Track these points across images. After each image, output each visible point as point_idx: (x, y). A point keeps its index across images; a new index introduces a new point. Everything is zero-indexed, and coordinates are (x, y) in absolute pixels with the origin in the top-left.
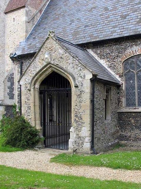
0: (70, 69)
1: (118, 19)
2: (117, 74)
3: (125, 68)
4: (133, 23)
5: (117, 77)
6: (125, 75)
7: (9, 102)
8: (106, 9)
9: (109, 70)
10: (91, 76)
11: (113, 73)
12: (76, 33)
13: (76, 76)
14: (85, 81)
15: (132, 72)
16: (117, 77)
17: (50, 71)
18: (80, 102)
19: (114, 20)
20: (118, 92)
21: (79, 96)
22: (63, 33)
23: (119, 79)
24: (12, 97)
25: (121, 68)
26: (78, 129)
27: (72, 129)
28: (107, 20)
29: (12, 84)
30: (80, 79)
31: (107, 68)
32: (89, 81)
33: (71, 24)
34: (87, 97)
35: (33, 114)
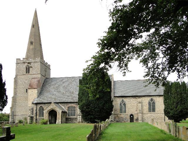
7: (32, 116)
26: (58, 121)
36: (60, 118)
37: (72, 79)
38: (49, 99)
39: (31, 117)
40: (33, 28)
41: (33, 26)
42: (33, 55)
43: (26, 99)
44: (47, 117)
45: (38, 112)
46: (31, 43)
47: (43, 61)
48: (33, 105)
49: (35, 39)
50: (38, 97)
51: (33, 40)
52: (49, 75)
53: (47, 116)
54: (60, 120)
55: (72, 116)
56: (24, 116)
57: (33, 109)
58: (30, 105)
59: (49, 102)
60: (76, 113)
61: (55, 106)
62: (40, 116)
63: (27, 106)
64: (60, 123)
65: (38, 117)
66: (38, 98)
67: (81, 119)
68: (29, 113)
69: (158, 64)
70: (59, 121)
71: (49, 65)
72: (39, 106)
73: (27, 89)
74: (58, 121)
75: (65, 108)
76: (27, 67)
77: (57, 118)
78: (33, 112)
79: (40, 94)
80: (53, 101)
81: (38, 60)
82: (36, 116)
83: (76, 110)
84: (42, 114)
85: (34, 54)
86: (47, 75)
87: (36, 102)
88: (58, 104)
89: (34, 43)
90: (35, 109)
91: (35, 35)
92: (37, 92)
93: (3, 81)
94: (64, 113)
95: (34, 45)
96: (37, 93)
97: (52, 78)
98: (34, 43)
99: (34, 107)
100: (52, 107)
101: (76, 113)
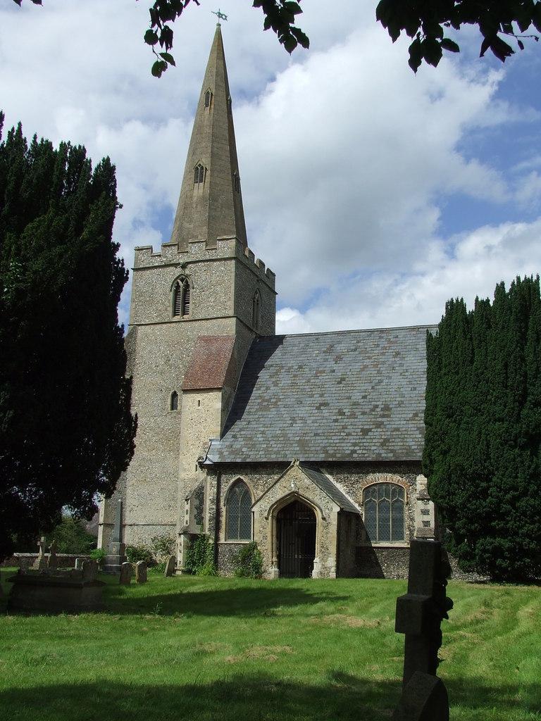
0: (317, 500)
1: (359, 434)
2: (356, 502)
3: (365, 496)
4: (376, 444)
5: (356, 506)
6: (366, 504)
7: (196, 530)
8: (341, 413)
9: (347, 496)
10: (338, 509)
11: (352, 501)
12: (303, 444)
13: (323, 508)
14: (332, 513)
15: (374, 501)
16: (356, 506)
17: (293, 499)
18: (327, 533)
19: (353, 434)
20: (229, 550)
21: (326, 527)
22: (282, 439)
23: (359, 509)
24: (199, 520)
25: (360, 494)
26: (323, 560)
27: (316, 560)
28: (344, 432)
29: (202, 502)
30: (327, 511)
31: (344, 493)
32: (336, 514)
33: (291, 425)
34: (333, 528)
35: (270, 545)
36: (333, 549)
37: (381, 338)
38: (276, 446)
39: (193, 538)
40: (207, 106)
41: (207, 98)
42: (205, 229)
43: (173, 440)
44: (269, 538)
45: (224, 509)
46: (197, 173)
47: (247, 253)
48: (202, 475)
49: (213, 155)
50: (226, 427)
51: (205, 161)
52: (274, 329)
53: (269, 535)
54: (331, 562)
55: (388, 539)
56: (160, 531)
57: (199, 494)
58: (190, 474)
59: (273, 458)
60: (406, 525)
61: (307, 481)
62: (230, 535)
63: (175, 474)
64: (333, 575)
65: (222, 535)
66: (223, 435)
67: (431, 518)
68: (182, 516)
69: (484, 84)
70: (325, 563)
71: (271, 275)
72: (229, 480)
73: (174, 395)
74: (323, 560)
75: (351, 492)
76: (178, 287)
77: (317, 546)
78: (200, 509)
79: (233, 414)
80: (293, 454)
81: (227, 247)
82: (217, 529)
83: (406, 508)
84: (241, 525)
85: (211, 221)
86: (260, 323)
87: (214, 458)
88: (318, 471)
89: (208, 173)
90: (210, 493)
91: (215, 138)
92: (219, 405)
93: (119, 324)
94: (347, 518)
95: (208, 180)
96: (223, 410)
97: (282, 338)
98: (208, 173)
99: (210, 483)
100: (296, 482)
101: (407, 523)
